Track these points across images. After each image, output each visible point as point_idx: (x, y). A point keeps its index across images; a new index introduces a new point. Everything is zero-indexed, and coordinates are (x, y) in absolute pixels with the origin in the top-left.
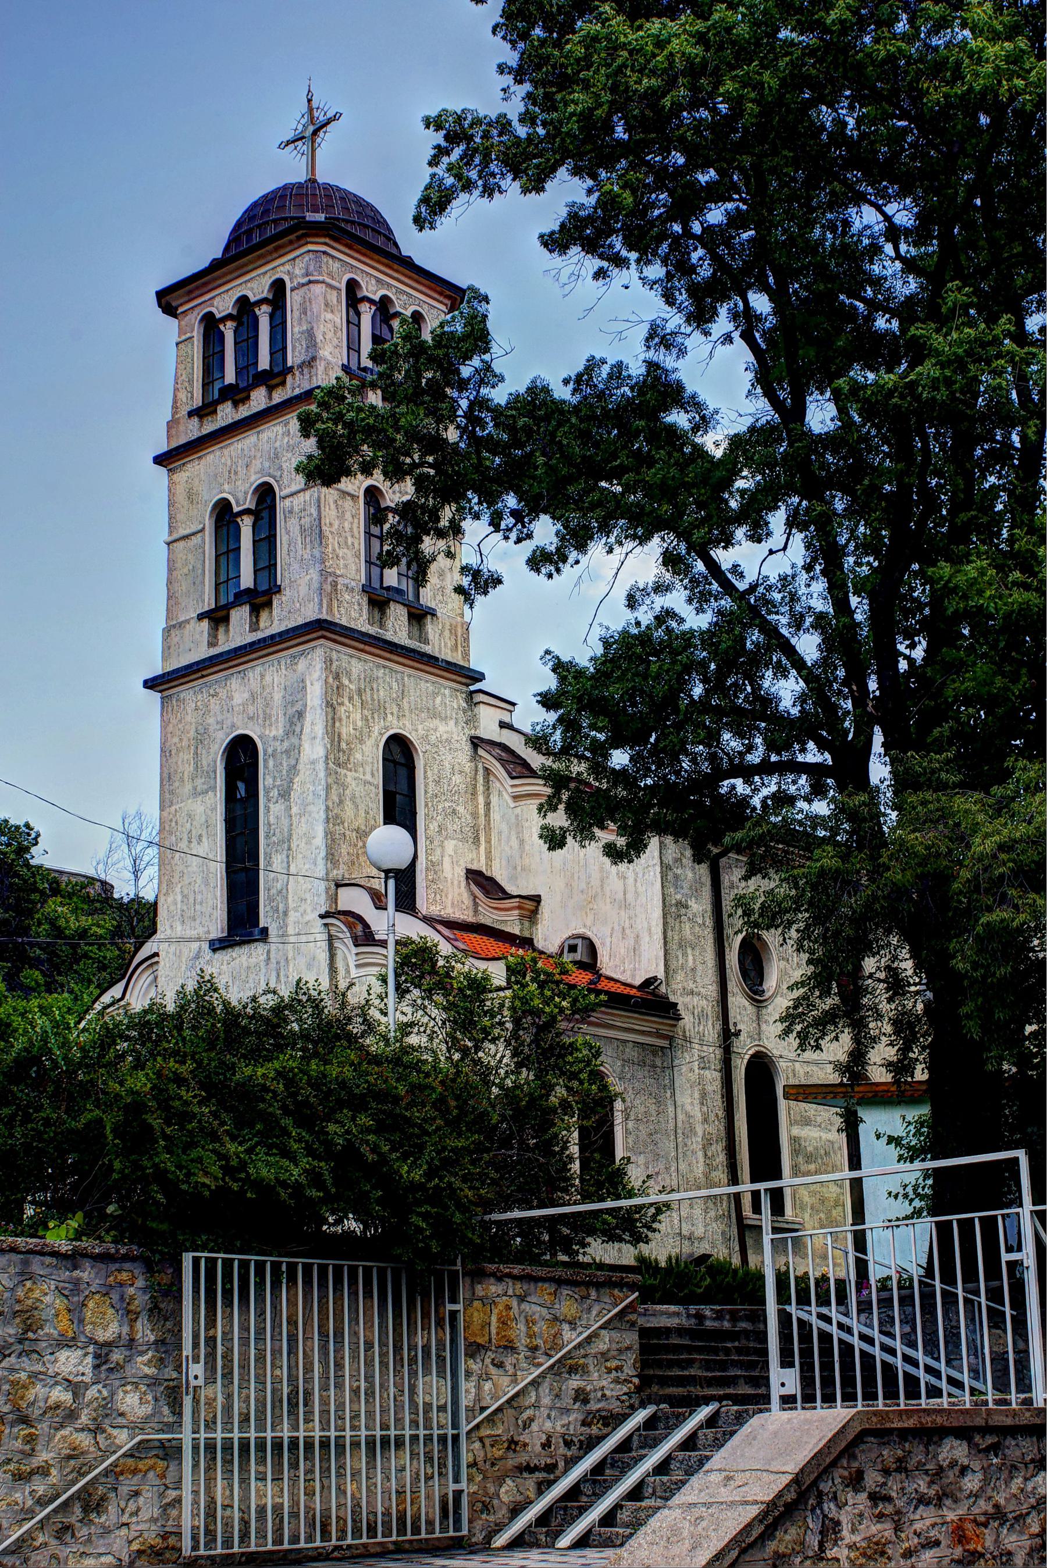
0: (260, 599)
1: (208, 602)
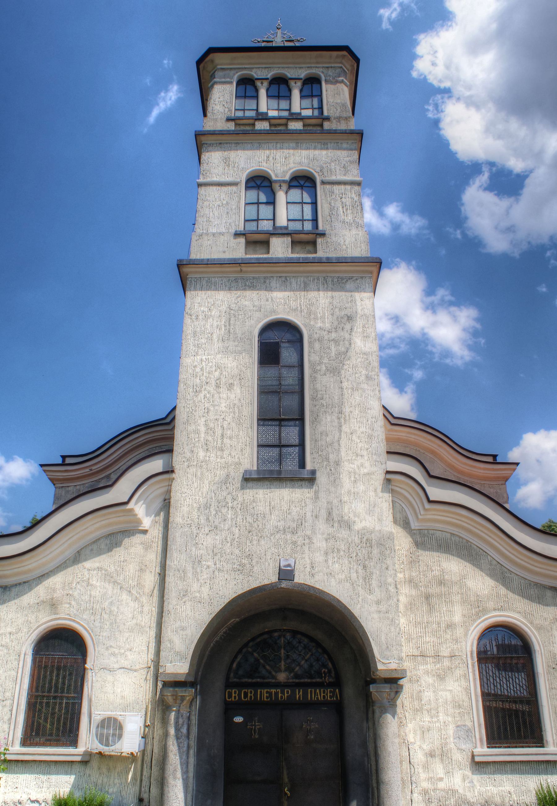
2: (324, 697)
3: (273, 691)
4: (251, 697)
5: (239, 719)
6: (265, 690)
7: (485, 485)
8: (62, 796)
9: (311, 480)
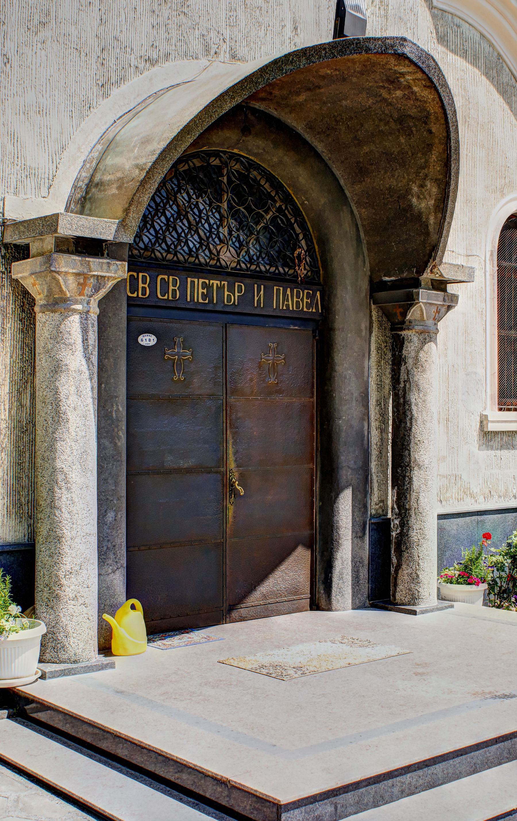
2: (298, 303)
3: (215, 283)
4: (174, 291)
6: (201, 281)
8: (7, 540)
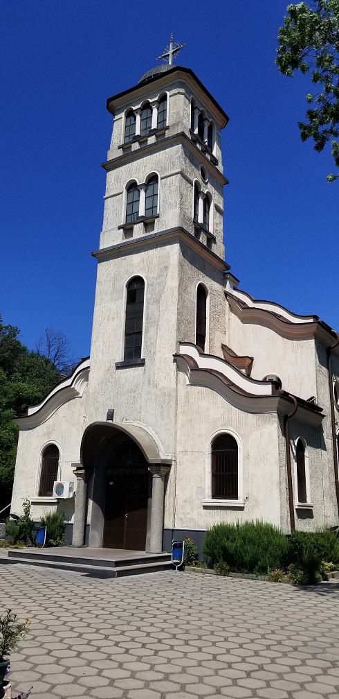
0: (149, 223)
1: (122, 222)
5: (111, 483)
7: (220, 354)
9: (142, 364)
